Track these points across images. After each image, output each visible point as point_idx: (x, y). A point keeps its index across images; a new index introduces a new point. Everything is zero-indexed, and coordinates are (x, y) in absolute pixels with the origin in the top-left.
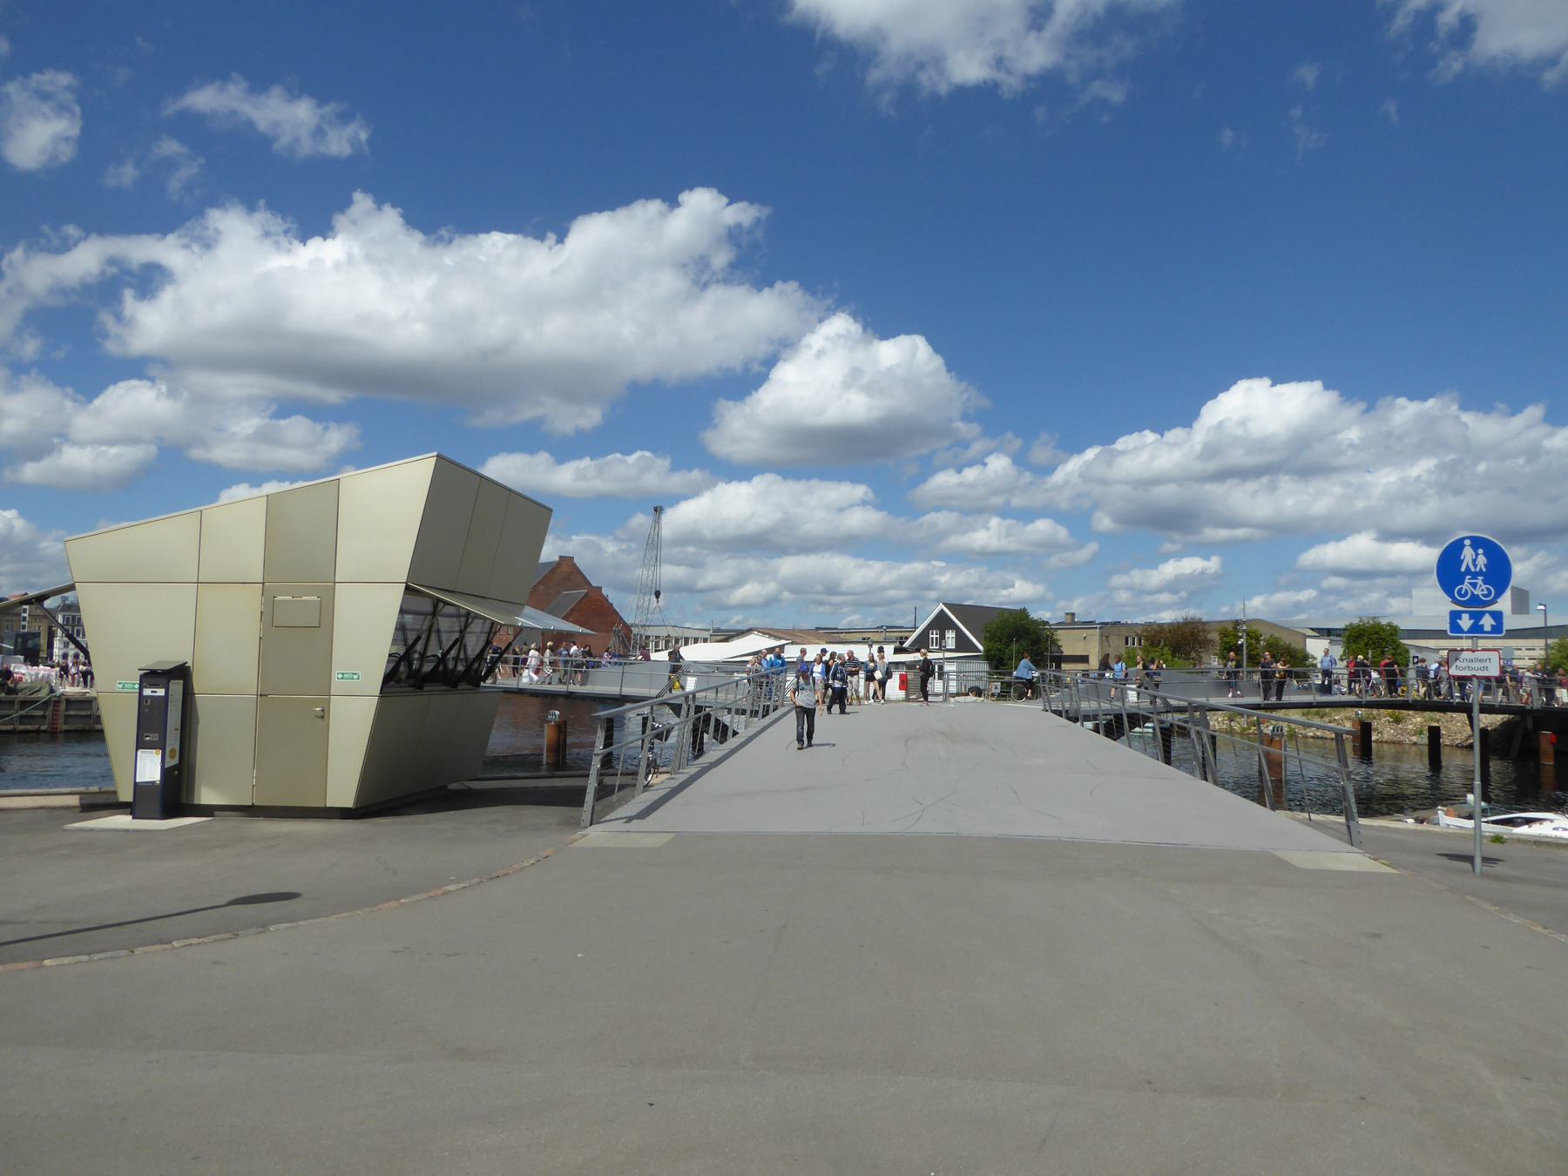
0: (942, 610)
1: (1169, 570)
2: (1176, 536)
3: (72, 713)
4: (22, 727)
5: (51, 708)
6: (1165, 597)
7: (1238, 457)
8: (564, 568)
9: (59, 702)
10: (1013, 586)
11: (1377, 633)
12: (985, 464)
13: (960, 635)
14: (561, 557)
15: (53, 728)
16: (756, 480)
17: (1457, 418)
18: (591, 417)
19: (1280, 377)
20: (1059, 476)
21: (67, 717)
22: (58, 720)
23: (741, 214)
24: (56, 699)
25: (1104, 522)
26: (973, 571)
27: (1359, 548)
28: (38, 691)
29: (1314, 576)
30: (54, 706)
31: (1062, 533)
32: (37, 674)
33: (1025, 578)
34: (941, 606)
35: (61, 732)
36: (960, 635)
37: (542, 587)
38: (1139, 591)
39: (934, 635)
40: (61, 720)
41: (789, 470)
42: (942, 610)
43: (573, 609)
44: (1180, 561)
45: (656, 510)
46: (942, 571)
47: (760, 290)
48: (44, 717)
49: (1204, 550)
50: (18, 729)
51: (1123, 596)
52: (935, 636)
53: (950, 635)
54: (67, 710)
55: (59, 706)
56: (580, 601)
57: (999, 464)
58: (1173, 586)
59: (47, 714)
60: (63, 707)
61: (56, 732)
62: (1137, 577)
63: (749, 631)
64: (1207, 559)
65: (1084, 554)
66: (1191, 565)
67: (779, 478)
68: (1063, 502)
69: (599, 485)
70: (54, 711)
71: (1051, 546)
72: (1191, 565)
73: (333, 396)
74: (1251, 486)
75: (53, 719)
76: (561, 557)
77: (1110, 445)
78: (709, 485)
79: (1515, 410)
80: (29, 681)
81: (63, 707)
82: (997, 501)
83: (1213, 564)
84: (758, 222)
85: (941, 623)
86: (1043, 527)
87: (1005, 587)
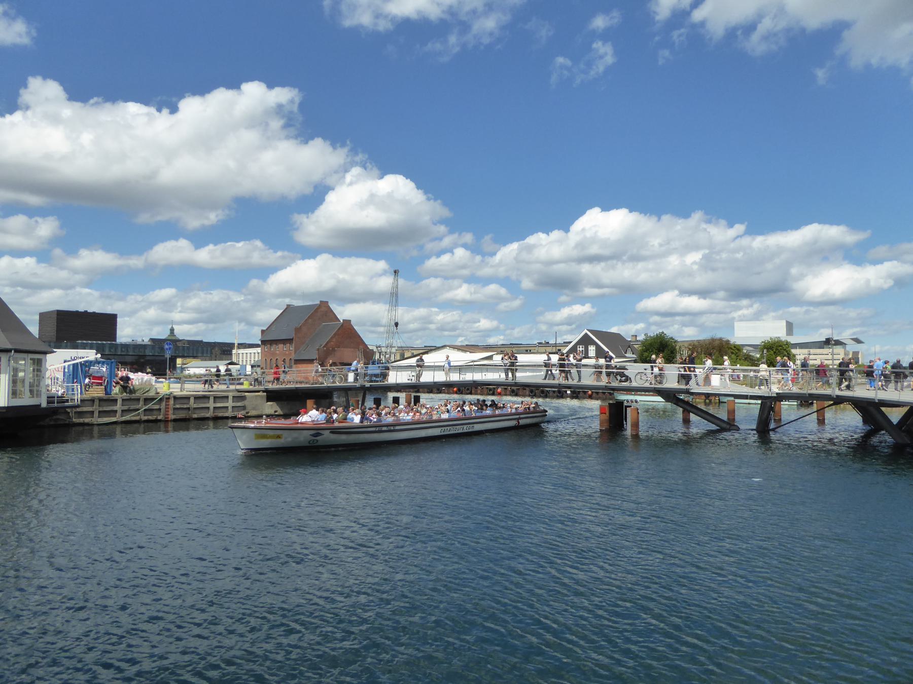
0: (586, 334)
1: (565, 312)
2: (566, 291)
3: (178, 406)
4: (146, 418)
5: (164, 404)
6: (565, 328)
7: (594, 250)
8: (323, 309)
9: (169, 398)
10: (479, 322)
11: (780, 346)
12: (453, 253)
13: (598, 348)
14: (321, 301)
15: (166, 418)
16: (319, 258)
17: (705, 230)
18: (213, 217)
19: (606, 207)
20: (498, 257)
21: (174, 409)
22: (168, 411)
23: (282, 95)
24: (168, 397)
25: (526, 284)
26: (454, 313)
27: (665, 300)
28: (148, 391)
29: (644, 315)
30: (166, 402)
31: (503, 291)
32: (142, 379)
33: (486, 318)
34: (586, 331)
35: (171, 421)
36: (598, 348)
37: (310, 320)
38: (551, 324)
39: (581, 348)
40: (171, 412)
41: (338, 252)
42: (586, 334)
43: (335, 335)
44: (343, 306)
45: (395, 272)
46: (437, 314)
47: (306, 143)
48: (160, 410)
49: (583, 300)
50: (143, 419)
51: (544, 327)
52: (581, 349)
53: (592, 350)
54: (174, 405)
55: (169, 402)
56: (339, 329)
57: (460, 253)
58: (569, 321)
59: (161, 407)
60: (172, 402)
61: (168, 421)
62: (549, 316)
63: (444, 347)
64: (583, 305)
65: (517, 303)
66: (578, 309)
67: (330, 256)
68: (502, 271)
69: (223, 261)
70: (166, 405)
71: (500, 299)
72: (578, 309)
73: (34, 200)
74: (603, 264)
75: (166, 411)
76: (321, 301)
77: (524, 240)
78: (293, 260)
79: (731, 225)
80: (137, 384)
81: (172, 402)
82: (465, 272)
83: (587, 308)
84: (292, 101)
85: (586, 341)
86: (493, 288)
87: (475, 322)
